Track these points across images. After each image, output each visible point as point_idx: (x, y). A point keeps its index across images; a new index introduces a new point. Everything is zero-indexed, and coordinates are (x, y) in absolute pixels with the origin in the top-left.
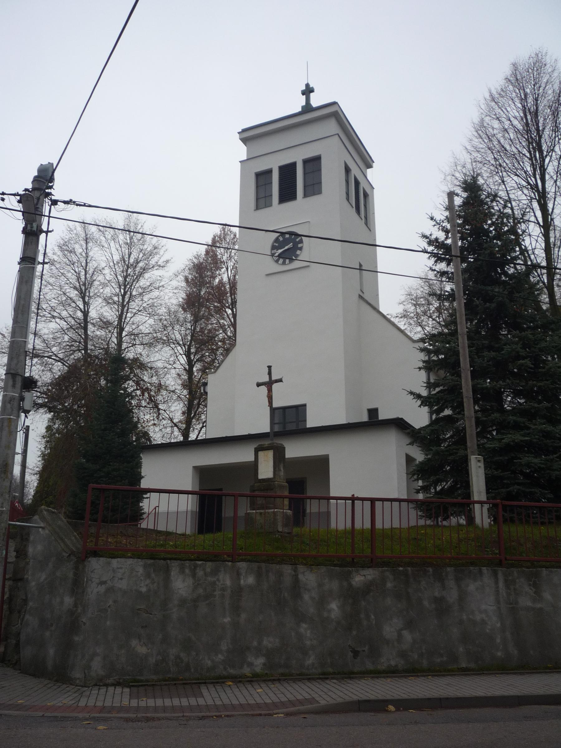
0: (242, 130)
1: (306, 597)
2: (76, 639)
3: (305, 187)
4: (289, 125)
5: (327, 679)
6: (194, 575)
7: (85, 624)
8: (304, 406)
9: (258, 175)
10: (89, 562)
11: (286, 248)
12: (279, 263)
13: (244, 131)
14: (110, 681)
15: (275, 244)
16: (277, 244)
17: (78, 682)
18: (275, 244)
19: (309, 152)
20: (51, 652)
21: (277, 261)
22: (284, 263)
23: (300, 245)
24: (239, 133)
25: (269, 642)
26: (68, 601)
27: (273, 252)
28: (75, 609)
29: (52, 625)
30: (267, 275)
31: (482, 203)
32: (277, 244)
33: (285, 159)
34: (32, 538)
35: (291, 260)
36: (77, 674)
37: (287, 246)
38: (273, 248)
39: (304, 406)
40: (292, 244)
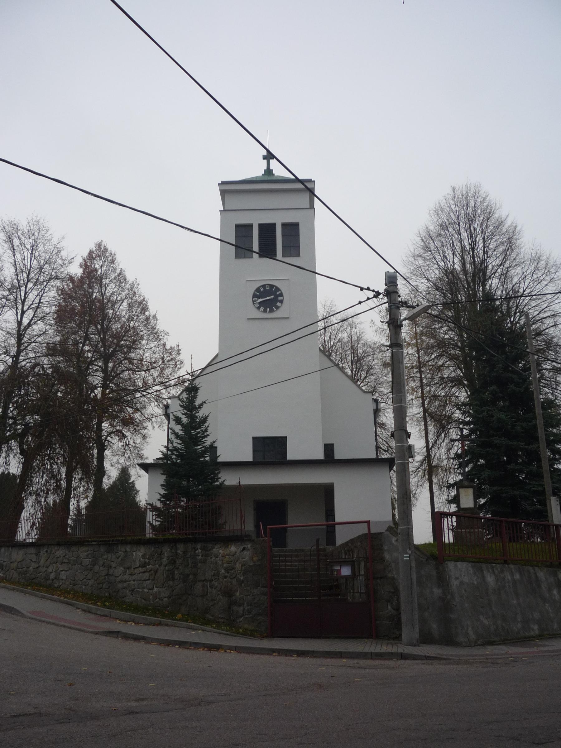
0: (222, 182)
1: (543, 586)
2: (452, 616)
3: (283, 247)
4: (268, 189)
5: (552, 638)
6: (494, 573)
7: (456, 606)
8: (285, 438)
9: (238, 227)
10: (447, 564)
11: (268, 298)
12: (260, 310)
13: (224, 183)
14: (479, 643)
15: (256, 293)
16: (258, 294)
17: (464, 644)
18: (256, 293)
19: (290, 218)
20: (434, 626)
21: (258, 308)
22: (265, 311)
23: (280, 298)
24: (219, 184)
25: (536, 615)
26: (437, 591)
27: (254, 299)
28: (444, 596)
29: (429, 608)
30: (249, 319)
31: (496, 310)
32: (258, 294)
33: (267, 219)
34: (386, 548)
35: (272, 311)
36: (461, 639)
37: (269, 296)
38: (254, 296)
39: (285, 438)
40: (273, 296)
